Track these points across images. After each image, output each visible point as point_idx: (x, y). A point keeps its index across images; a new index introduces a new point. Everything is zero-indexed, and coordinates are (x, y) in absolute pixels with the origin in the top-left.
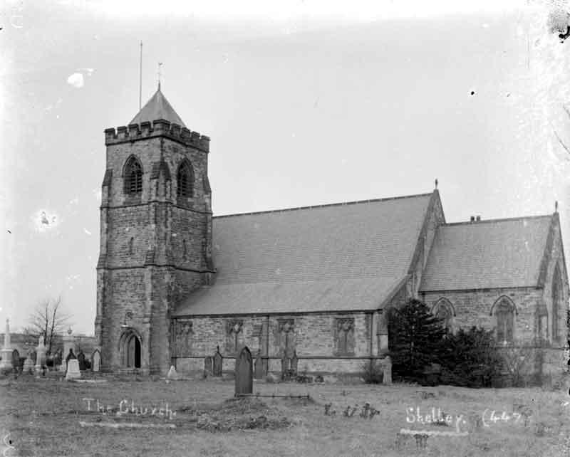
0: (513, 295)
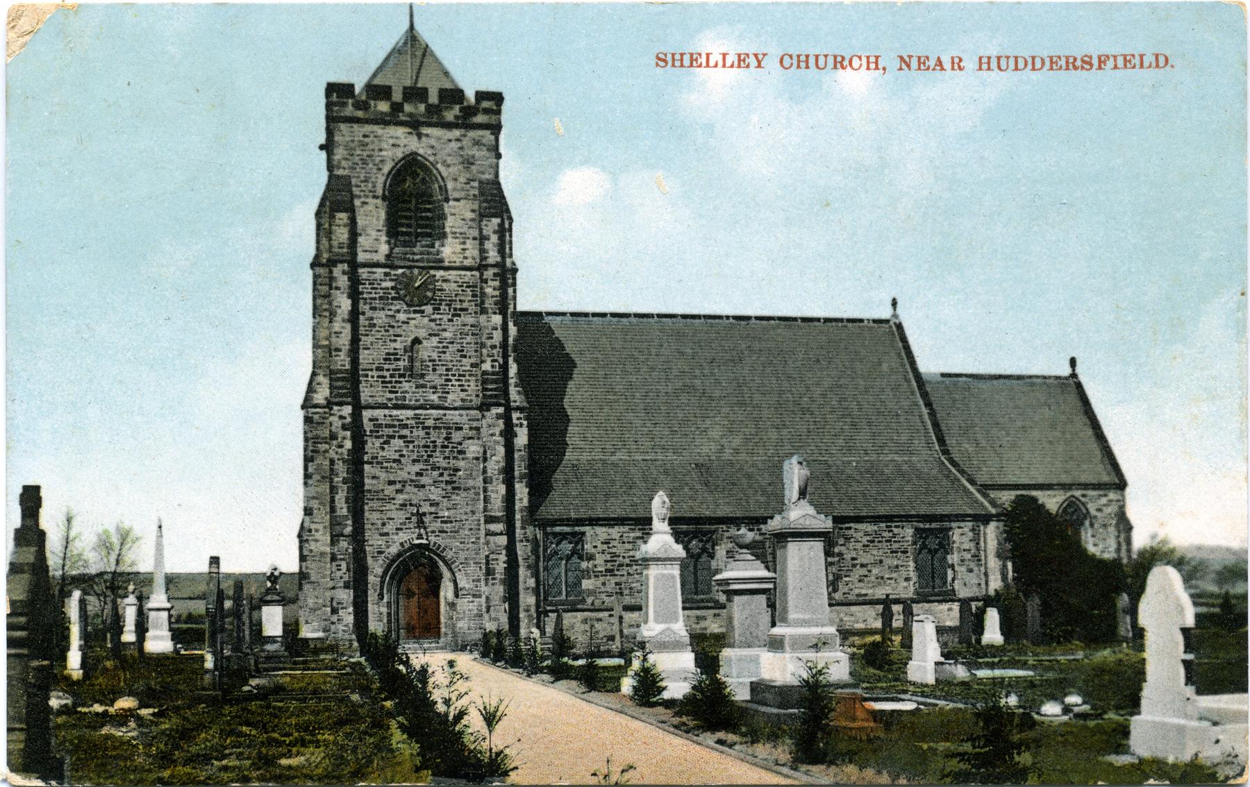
0: (1084, 496)
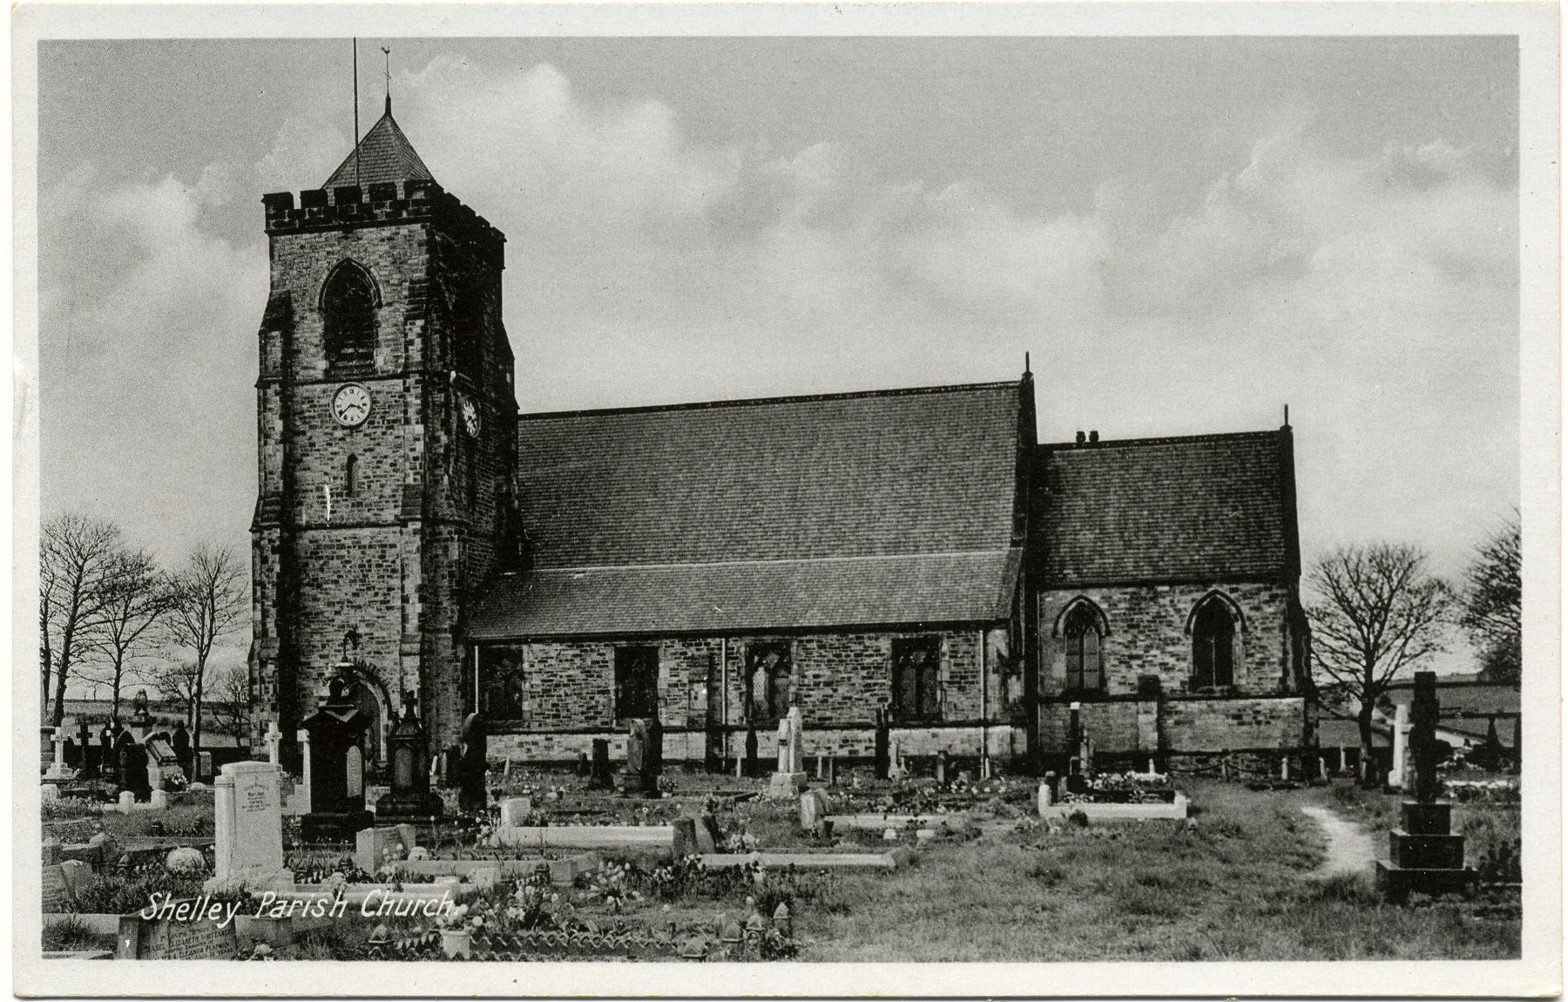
0: (1233, 591)
